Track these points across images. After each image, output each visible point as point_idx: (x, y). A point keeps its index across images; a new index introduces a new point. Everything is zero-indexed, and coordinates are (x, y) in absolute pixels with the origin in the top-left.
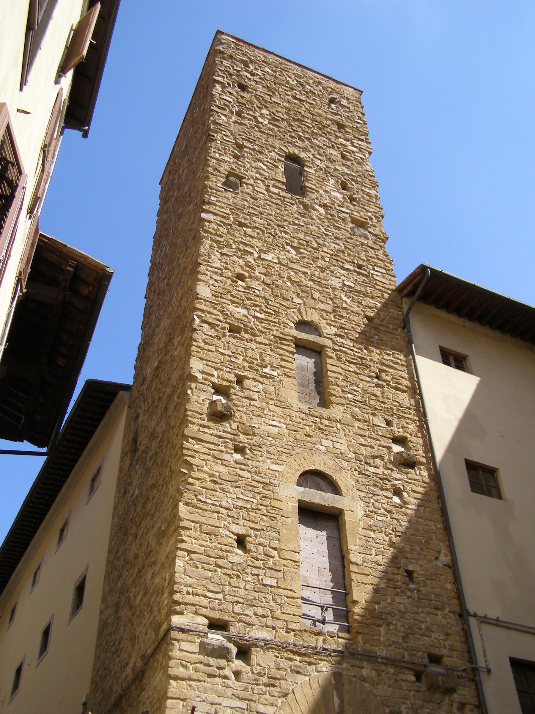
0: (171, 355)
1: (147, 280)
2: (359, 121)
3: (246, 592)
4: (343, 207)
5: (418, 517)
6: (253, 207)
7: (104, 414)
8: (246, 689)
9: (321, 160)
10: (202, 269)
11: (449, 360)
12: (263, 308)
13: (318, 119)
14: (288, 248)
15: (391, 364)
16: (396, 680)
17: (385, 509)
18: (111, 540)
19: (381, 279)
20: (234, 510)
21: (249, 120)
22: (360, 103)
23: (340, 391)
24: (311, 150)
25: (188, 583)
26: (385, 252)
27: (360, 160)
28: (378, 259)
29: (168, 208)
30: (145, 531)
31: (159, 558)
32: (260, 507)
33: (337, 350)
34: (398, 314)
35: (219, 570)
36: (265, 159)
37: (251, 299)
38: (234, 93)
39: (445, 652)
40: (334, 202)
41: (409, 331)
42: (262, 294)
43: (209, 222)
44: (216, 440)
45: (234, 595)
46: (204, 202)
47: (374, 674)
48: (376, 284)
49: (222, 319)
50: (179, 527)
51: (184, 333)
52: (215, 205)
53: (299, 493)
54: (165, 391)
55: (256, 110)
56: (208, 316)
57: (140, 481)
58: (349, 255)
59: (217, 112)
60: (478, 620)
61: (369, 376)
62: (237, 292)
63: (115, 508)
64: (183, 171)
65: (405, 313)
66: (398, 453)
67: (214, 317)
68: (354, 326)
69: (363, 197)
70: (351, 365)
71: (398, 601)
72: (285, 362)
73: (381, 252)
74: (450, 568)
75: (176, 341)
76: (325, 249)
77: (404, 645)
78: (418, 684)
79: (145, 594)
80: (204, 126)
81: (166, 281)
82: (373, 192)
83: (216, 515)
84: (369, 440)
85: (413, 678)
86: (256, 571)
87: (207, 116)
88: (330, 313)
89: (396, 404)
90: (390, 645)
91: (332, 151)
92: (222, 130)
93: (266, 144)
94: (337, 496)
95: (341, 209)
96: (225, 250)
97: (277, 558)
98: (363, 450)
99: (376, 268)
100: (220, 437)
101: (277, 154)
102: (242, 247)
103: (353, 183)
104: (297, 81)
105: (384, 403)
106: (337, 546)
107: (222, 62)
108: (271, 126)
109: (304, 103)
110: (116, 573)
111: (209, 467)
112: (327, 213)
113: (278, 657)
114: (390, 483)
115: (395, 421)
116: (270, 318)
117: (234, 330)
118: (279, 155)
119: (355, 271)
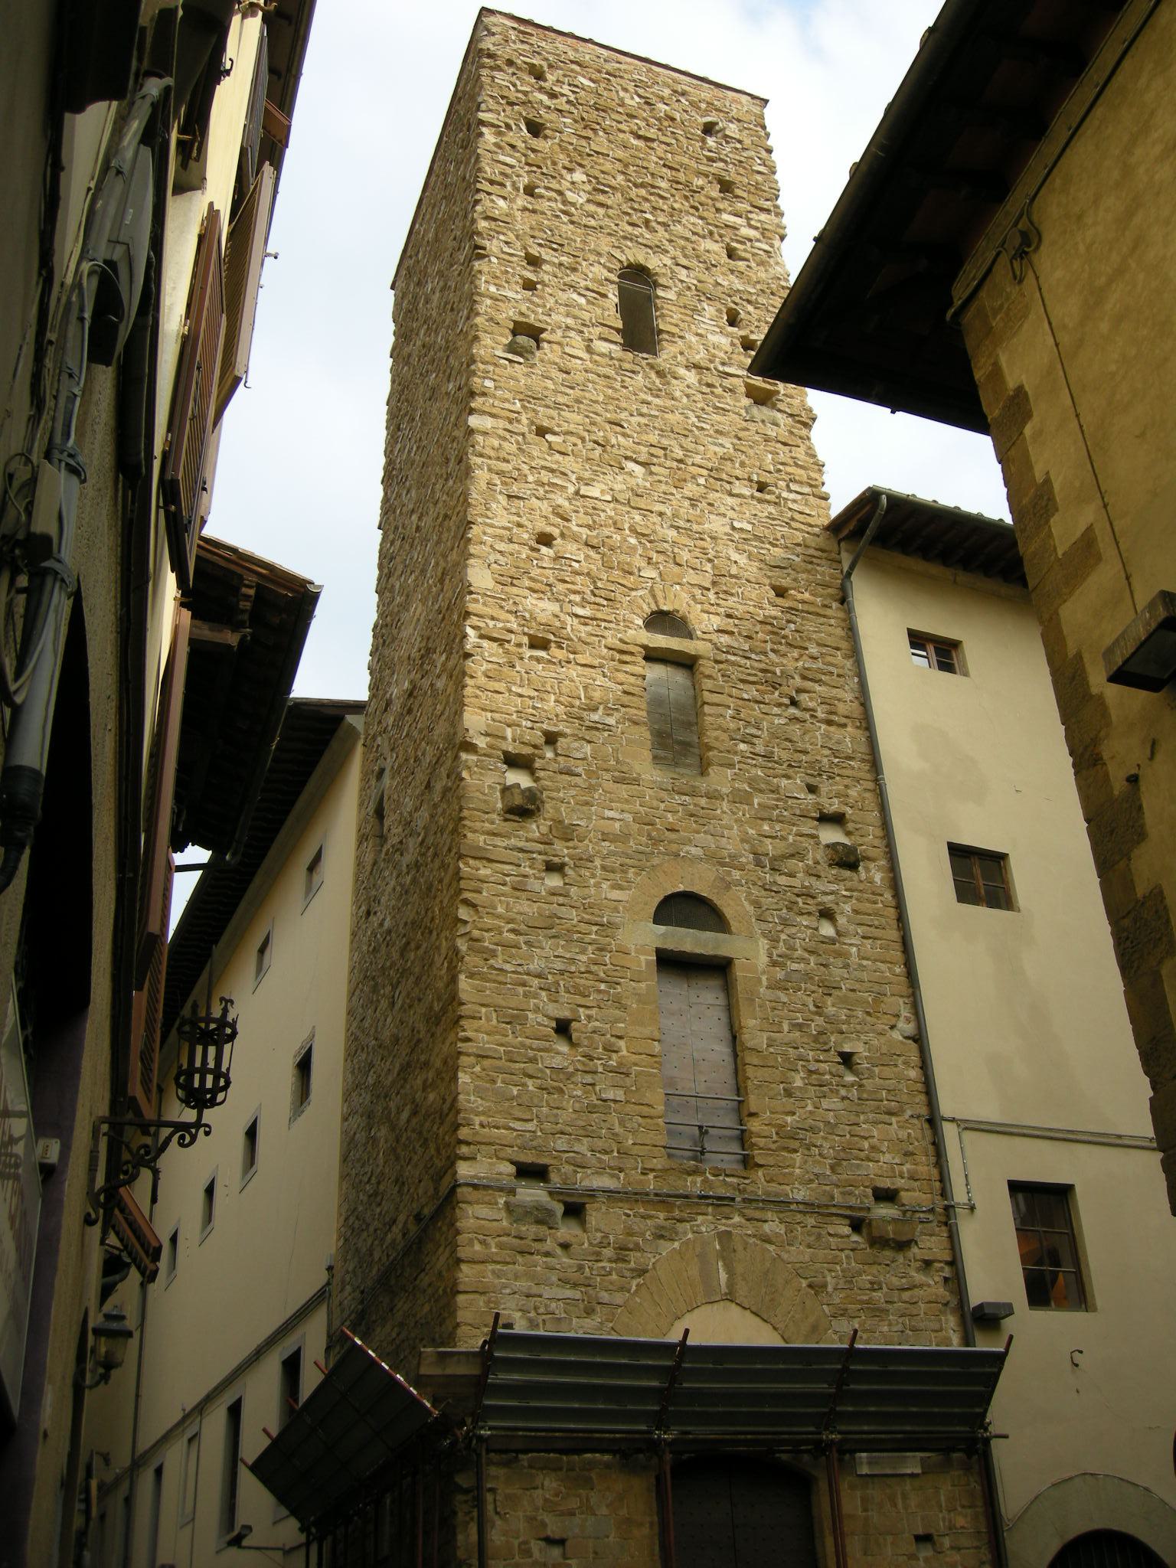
3: (574, 1116)
14: (630, 466)
16: (819, 1236)
32: (594, 968)
35: (530, 1082)
39: (900, 1183)
47: (781, 1229)
49: (515, 626)
50: (461, 1017)
56: (491, 623)
57: (393, 902)
61: (779, 705)
63: (354, 934)
66: (828, 846)
68: (751, 609)
78: (855, 1238)
83: (521, 990)
86: (588, 1079)
89: (827, 752)
90: (811, 1181)
97: (624, 1053)
100: (521, 850)
102: (545, 476)
105: (805, 752)
106: (725, 1019)
116: (599, 615)
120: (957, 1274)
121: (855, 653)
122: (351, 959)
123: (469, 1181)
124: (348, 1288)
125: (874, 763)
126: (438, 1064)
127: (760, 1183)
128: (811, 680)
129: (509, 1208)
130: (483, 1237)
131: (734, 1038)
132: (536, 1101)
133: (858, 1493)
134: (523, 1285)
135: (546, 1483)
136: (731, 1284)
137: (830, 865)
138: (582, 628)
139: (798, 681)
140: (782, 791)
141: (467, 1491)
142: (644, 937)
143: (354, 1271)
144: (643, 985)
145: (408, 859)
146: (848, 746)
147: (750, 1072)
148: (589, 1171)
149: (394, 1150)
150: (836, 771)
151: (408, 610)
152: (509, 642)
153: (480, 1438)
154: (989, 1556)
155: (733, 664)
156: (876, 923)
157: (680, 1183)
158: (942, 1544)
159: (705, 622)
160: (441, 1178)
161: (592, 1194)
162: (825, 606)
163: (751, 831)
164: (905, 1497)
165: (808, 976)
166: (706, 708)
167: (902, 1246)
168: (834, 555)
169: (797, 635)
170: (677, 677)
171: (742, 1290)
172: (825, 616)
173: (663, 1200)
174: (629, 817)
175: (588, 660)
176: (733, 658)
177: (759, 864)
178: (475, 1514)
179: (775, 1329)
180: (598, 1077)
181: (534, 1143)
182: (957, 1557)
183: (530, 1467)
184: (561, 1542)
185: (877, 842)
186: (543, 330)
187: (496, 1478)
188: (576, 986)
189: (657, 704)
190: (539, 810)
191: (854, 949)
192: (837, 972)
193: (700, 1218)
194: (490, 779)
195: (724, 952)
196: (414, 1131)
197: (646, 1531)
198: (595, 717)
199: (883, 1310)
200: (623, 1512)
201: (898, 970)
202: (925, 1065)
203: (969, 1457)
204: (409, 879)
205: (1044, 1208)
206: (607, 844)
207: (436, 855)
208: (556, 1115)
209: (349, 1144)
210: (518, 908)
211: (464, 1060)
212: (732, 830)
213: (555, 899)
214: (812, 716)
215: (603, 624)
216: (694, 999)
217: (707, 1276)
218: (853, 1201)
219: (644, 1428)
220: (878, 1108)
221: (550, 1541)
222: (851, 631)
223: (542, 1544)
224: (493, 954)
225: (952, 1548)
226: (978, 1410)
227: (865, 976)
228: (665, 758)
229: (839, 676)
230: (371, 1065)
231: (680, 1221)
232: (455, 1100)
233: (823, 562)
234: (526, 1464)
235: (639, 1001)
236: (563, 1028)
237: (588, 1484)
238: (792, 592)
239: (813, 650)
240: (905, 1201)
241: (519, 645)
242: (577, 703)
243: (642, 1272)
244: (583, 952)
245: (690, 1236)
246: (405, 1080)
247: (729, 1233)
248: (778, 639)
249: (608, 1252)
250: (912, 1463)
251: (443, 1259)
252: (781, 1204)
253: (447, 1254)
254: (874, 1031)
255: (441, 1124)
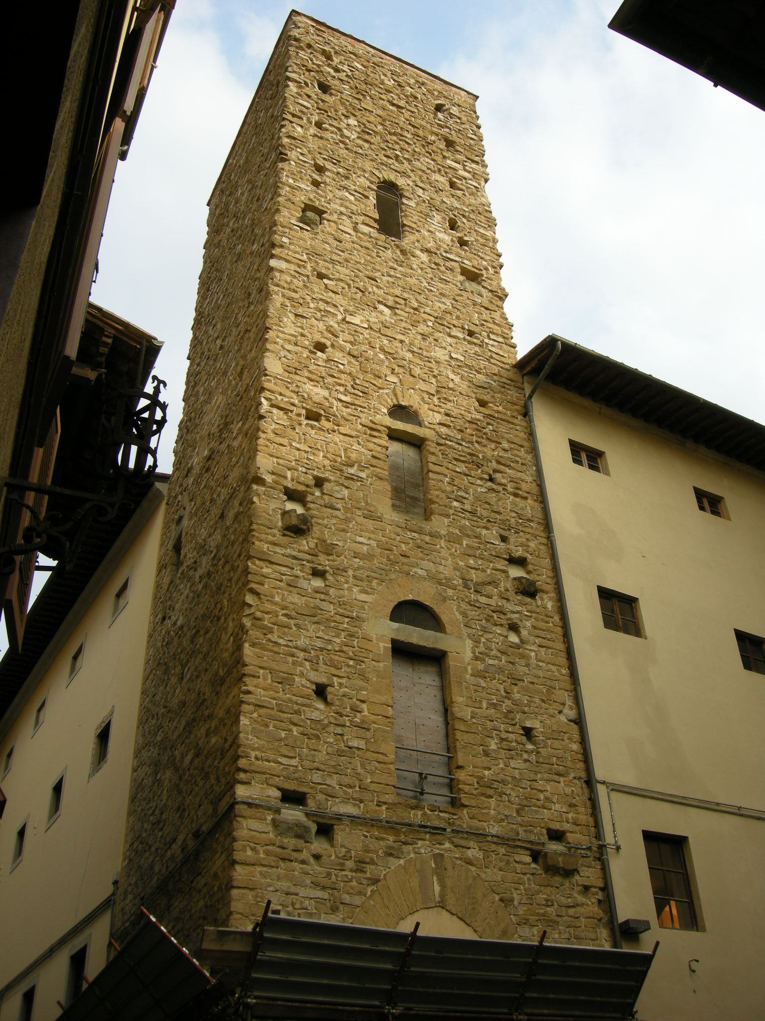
0: (229, 446)
1: (190, 335)
2: (473, 137)
4: (451, 253)
5: (540, 661)
6: (337, 251)
9: (423, 189)
10: (270, 335)
12: (349, 388)
13: (421, 133)
14: (381, 307)
16: (508, 862)
18: (146, 679)
19: (497, 351)
20: (312, 652)
21: (332, 132)
22: (475, 112)
24: (412, 175)
26: (503, 313)
27: (474, 190)
28: (494, 323)
29: (220, 241)
30: (195, 674)
33: (441, 445)
34: (518, 398)
36: (353, 187)
37: (333, 377)
38: (313, 95)
39: (566, 826)
40: (440, 246)
42: (348, 369)
43: (281, 271)
46: (273, 245)
47: (480, 855)
48: (491, 357)
49: (296, 402)
50: (244, 675)
51: (247, 419)
52: (289, 249)
55: (341, 119)
56: (280, 398)
58: (458, 318)
59: (291, 122)
60: (607, 787)
61: (481, 479)
62: (315, 367)
64: (242, 194)
65: (527, 395)
66: (515, 579)
67: (287, 400)
68: (463, 412)
69: (477, 240)
73: (498, 314)
76: (428, 310)
77: (519, 819)
79: (197, 755)
80: (273, 138)
81: (219, 342)
82: (489, 233)
83: (290, 659)
85: (528, 859)
87: (277, 126)
89: (514, 515)
90: (503, 820)
91: (437, 177)
92: (297, 147)
93: (354, 167)
94: (439, 634)
95: (448, 256)
96: (300, 311)
98: (473, 575)
99: (492, 336)
100: (295, 558)
101: (368, 179)
102: (322, 306)
103: (465, 220)
104: (395, 80)
105: (499, 513)
106: (439, 696)
107: (297, 53)
108: (360, 142)
109: (404, 111)
110: (154, 722)
112: (430, 261)
113: (366, 837)
114: (506, 617)
115: (512, 539)
116: (357, 402)
117: (313, 416)
118: (371, 182)
119: (464, 339)
161: (339, 817)
186: (325, 212)
224: (271, 631)
244: (338, 636)
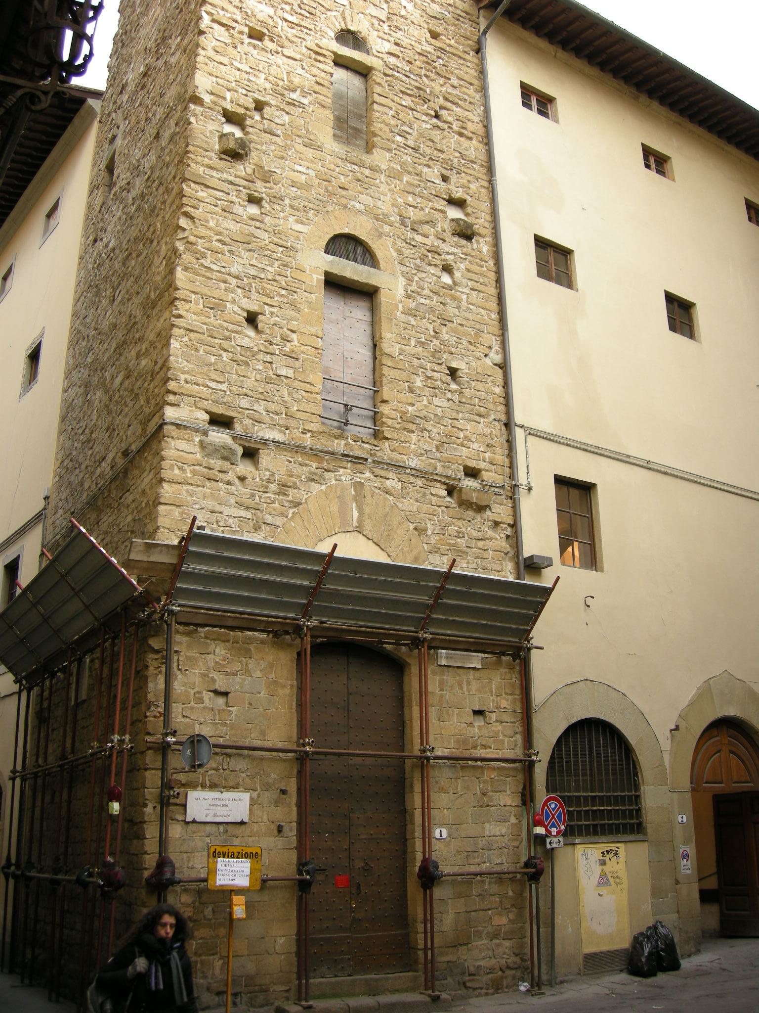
3: (256, 384)
7: (64, 128)
8: (252, 496)
11: (530, 101)
15: (456, 100)
16: (424, 495)
17: (431, 291)
20: (245, 279)
23: (388, 131)
25: (186, 369)
30: (127, 296)
31: (146, 334)
32: (278, 278)
33: (389, 76)
35: (224, 354)
39: (482, 465)
41: (482, 60)
44: (225, 186)
45: (241, 390)
47: (399, 486)
49: (239, 18)
50: (176, 299)
51: (187, 34)
53: (327, 262)
54: (156, 111)
56: (222, 13)
57: (119, 228)
61: (427, 115)
63: (81, 258)
65: (482, 30)
66: (453, 220)
68: (413, 43)
70: (405, 97)
71: (435, 403)
72: (320, 87)
74: (501, 368)
75: (174, 42)
77: (438, 455)
78: (448, 499)
83: (222, 285)
84: (419, 200)
86: (268, 358)
88: (384, 22)
89: (457, 154)
90: (422, 455)
94: (372, 270)
97: (296, 343)
100: (231, 183)
105: (443, 152)
106: (369, 331)
110: (84, 343)
111: (215, 222)
116: (303, 23)
117: (256, 35)
120: (516, 532)
121: (484, 90)
122: (78, 276)
123: (174, 421)
124: (61, 512)
125: (490, 170)
126: (152, 336)
127: (385, 451)
128: (451, 102)
129: (202, 445)
130: (182, 464)
131: (375, 346)
132: (228, 368)
133: (438, 678)
134: (210, 504)
135: (217, 650)
136: (360, 521)
137: (453, 234)
138: (289, 30)
139: (441, 101)
140: (423, 175)
141: (157, 652)
142: (317, 262)
143: (66, 499)
144: (313, 296)
145: (134, 193)
146: (472, 154)
147: (385, 370)
148: (264, 426)
149: (107, 406)
150: (462, 169)
151: (147, 15)
152: (234, 28)
153: (171, 612)
154: (521, 729)
155: (397, 78)
156: (481, 280)
157: (329, 443)
158: (490, 718)
159: (379, 44)
160: (149, 421)
161: (265, 442)
162: (466, 52)
163: (399, 200)
164: (468, 683)
165: (431, 310)
166: (375, 106)
167: (481, 509)
168: (474, 18)
169: (444, 68)
170: (356, 81)
171: (368, 527)
172: (464, 59)
173: (315, 454)
174: (312, 173)
175: (292, 55)
176: (397, 74)
177: (403, 224)
178: (163, 669)
179: (389, 556)
180: (275, 358)
181: (225, 400)
182: (500, 728)
183: (206, 638)
184: (226, 694)
185: (487, 224)
187: (180, 643)
188: (263, 288)
189: (339, 97)
190: (246, 154)
191: (464, 297)
192: (451, 311)
193: (342, 470)
194: (211, 126)
195: (374, 282)
196: (126, 390)
197: (287, 691)
198: (294, 96)
199: (464, 552)
200: (272, 676)
201: (493, 316)
202: (506, 385)
203: (514, 660)
204: (133, 208)
205: (575, 493)
206: (295, 189)
207: (161, 184)
208: (242, 382)
209: (68, 409)
210: (225, 224)
211: (175, 331)
212: (386, 198)
213: (253, 223)
214: (449, 127)
215: (305, 31)
216: (348, 314)
217: (344, 512)
218: (449, 473)
219: (293, 615)
220: (472, 410)
221: (217, 693)
222: (482, 73)
223: (212, 694)
225: (497, 721)
226: (526, 627)
227: (470, 316)
228: (341, 137)
229: (470, 103)
230: (91, 349)
231: (327, 470)
232: (167, 360)
233: (467, 21)
234: (203, 635)
235: (309, 307)
236: (252, 319)
237: (248, 653)
238: (443, 37)
239: (455, 81)
240: (485, 478)
241: (241, 33)
242: (281, 83)
243: (297, 504)
244: (271, 265)
245: (334, 482)
246: (120, 354)
247: (362, 483)
248: (430, 68)
249: (273, 487)
250: (476, 660)
251: (146, 481)
252: (399, 467)
253: (151, 475)
254: (473, 356)
255: (151, 381)
